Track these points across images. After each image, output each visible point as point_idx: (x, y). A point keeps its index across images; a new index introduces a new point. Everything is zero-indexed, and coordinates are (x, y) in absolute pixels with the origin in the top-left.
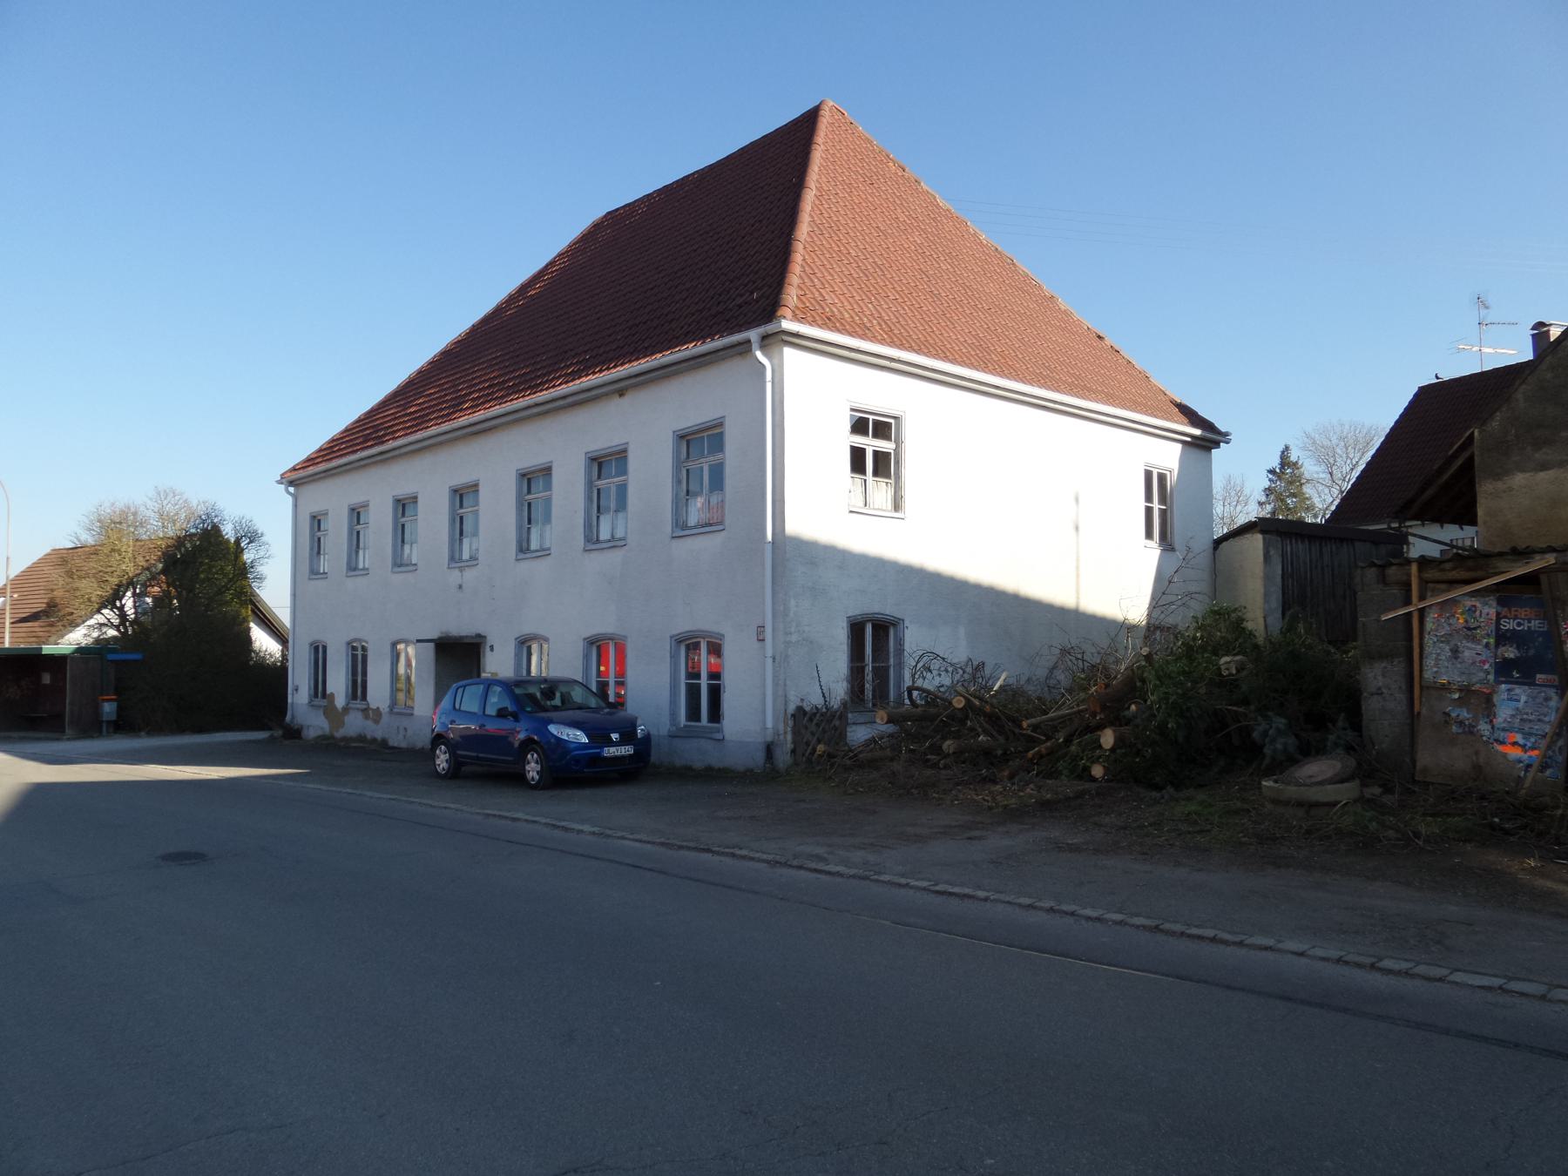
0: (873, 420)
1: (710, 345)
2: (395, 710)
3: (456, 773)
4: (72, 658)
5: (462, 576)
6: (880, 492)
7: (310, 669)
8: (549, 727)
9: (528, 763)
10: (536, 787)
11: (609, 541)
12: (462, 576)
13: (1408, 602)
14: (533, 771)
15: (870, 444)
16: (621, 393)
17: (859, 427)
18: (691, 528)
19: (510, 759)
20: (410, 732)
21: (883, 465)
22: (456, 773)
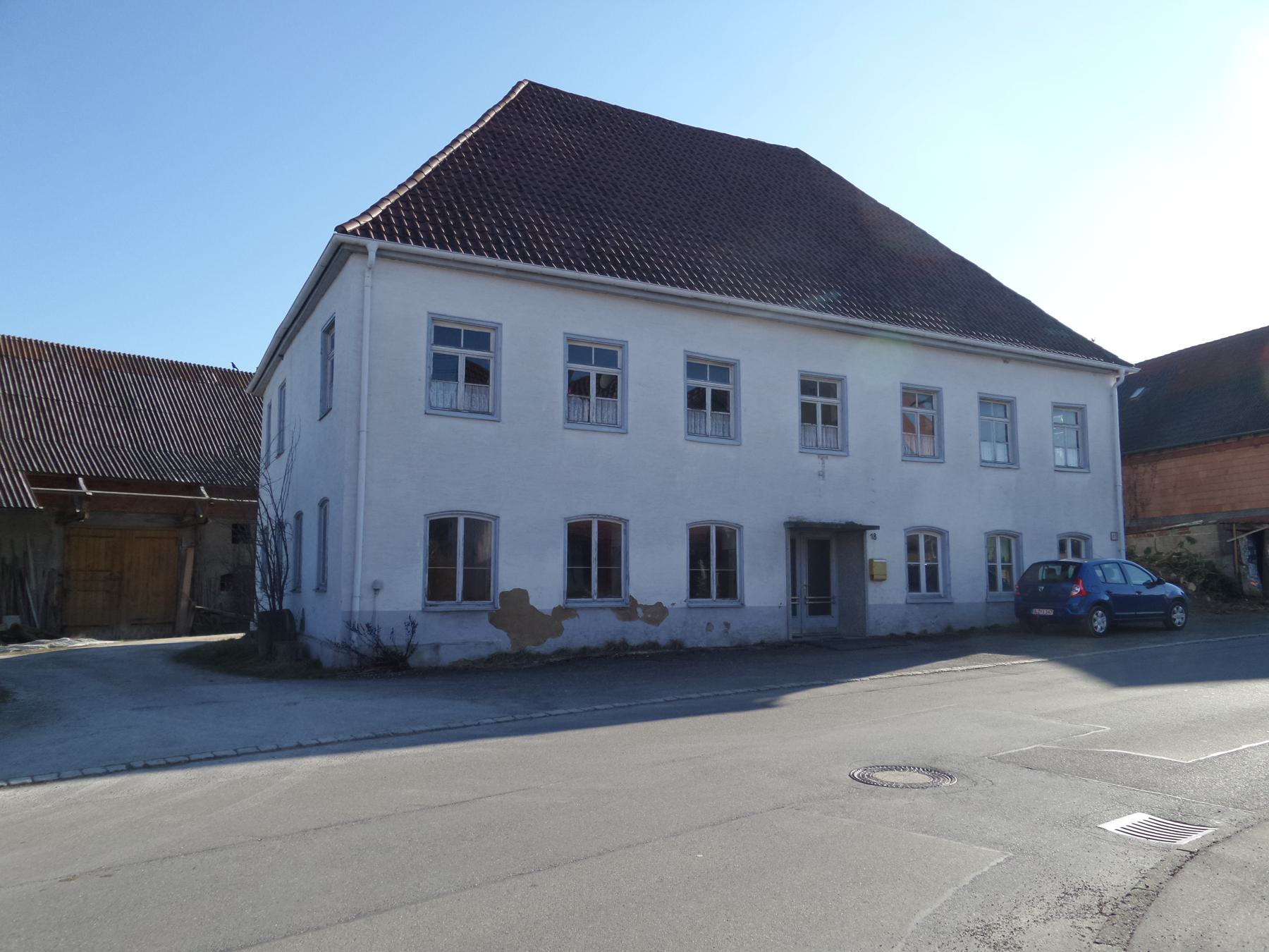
0: (595, 349)
1: (1039, 352)
2: (1156, 579)
3: (1115, 629)
4: (257, 506)
5: (823, 463)
6: (926, 447)
7: (565, 543)
8: (563, 622)
9: (1174, 613)
10: (1100, 635)
11: (990, 462)
12: (823, 463)
13: (1232, 537)
14: (1178, 618)
15: (819, 401)
16: (1006, 360)
17: (807, 386)
18: (1070, 467)
19: (1162, 612)
20: (733, 628)
21: (830, 416)
22: (1115, 629)
